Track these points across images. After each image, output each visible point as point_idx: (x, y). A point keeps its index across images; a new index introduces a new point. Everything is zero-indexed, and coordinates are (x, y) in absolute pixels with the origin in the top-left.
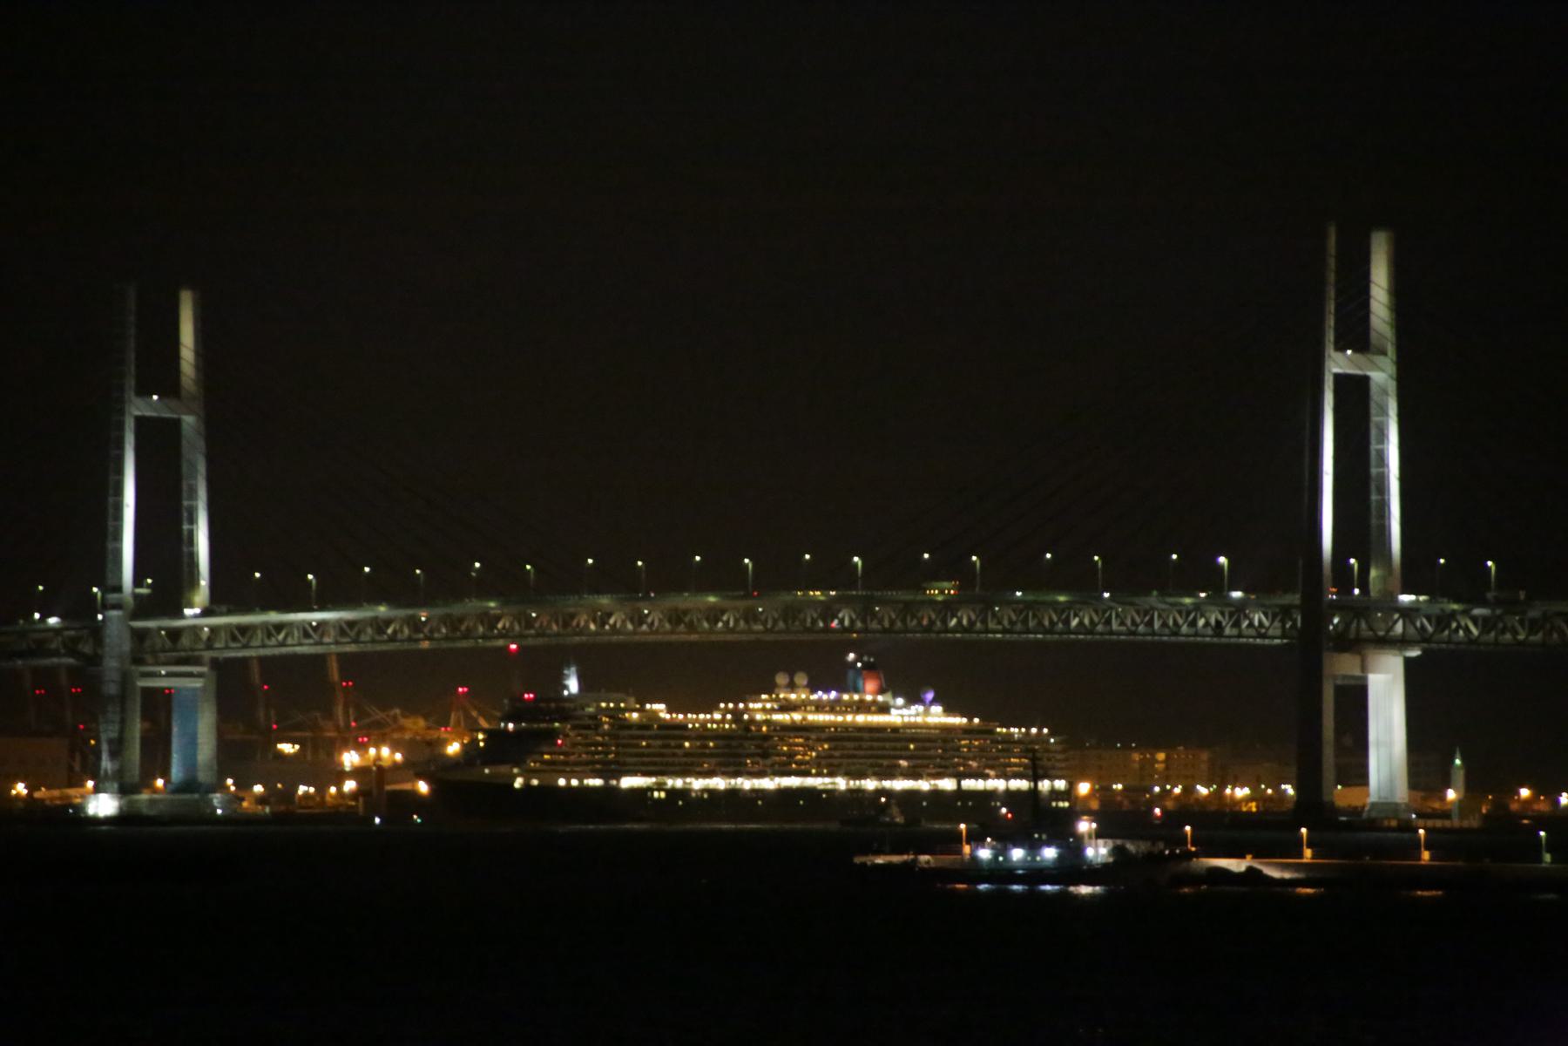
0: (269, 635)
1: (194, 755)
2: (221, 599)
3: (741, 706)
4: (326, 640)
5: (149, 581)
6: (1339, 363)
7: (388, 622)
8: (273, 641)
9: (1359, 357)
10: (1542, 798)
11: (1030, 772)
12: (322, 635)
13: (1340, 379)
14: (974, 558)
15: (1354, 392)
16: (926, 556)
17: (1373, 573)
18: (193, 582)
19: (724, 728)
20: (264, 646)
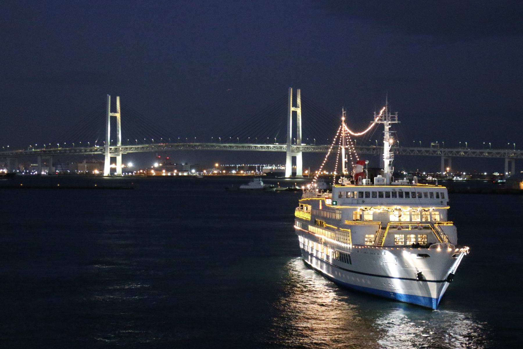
0: (130, 149)
1: (427, 308)
2: (123, 144)
3: (248, 172)
4: (139, 150)
5: (352, 163)
6: (292, 109)
7: (148, 147)
8: (131, 150)
9: (295, 108)
10: (105, 146)
11: (418, 216)
12: (138, 149)
13: (293, 111)
14: (490, 143)
15: (295, 113)
16: (308, 139)
17: (298, 141)
18: (119, 141)
19: (222, 173)
20: (129, 151)
